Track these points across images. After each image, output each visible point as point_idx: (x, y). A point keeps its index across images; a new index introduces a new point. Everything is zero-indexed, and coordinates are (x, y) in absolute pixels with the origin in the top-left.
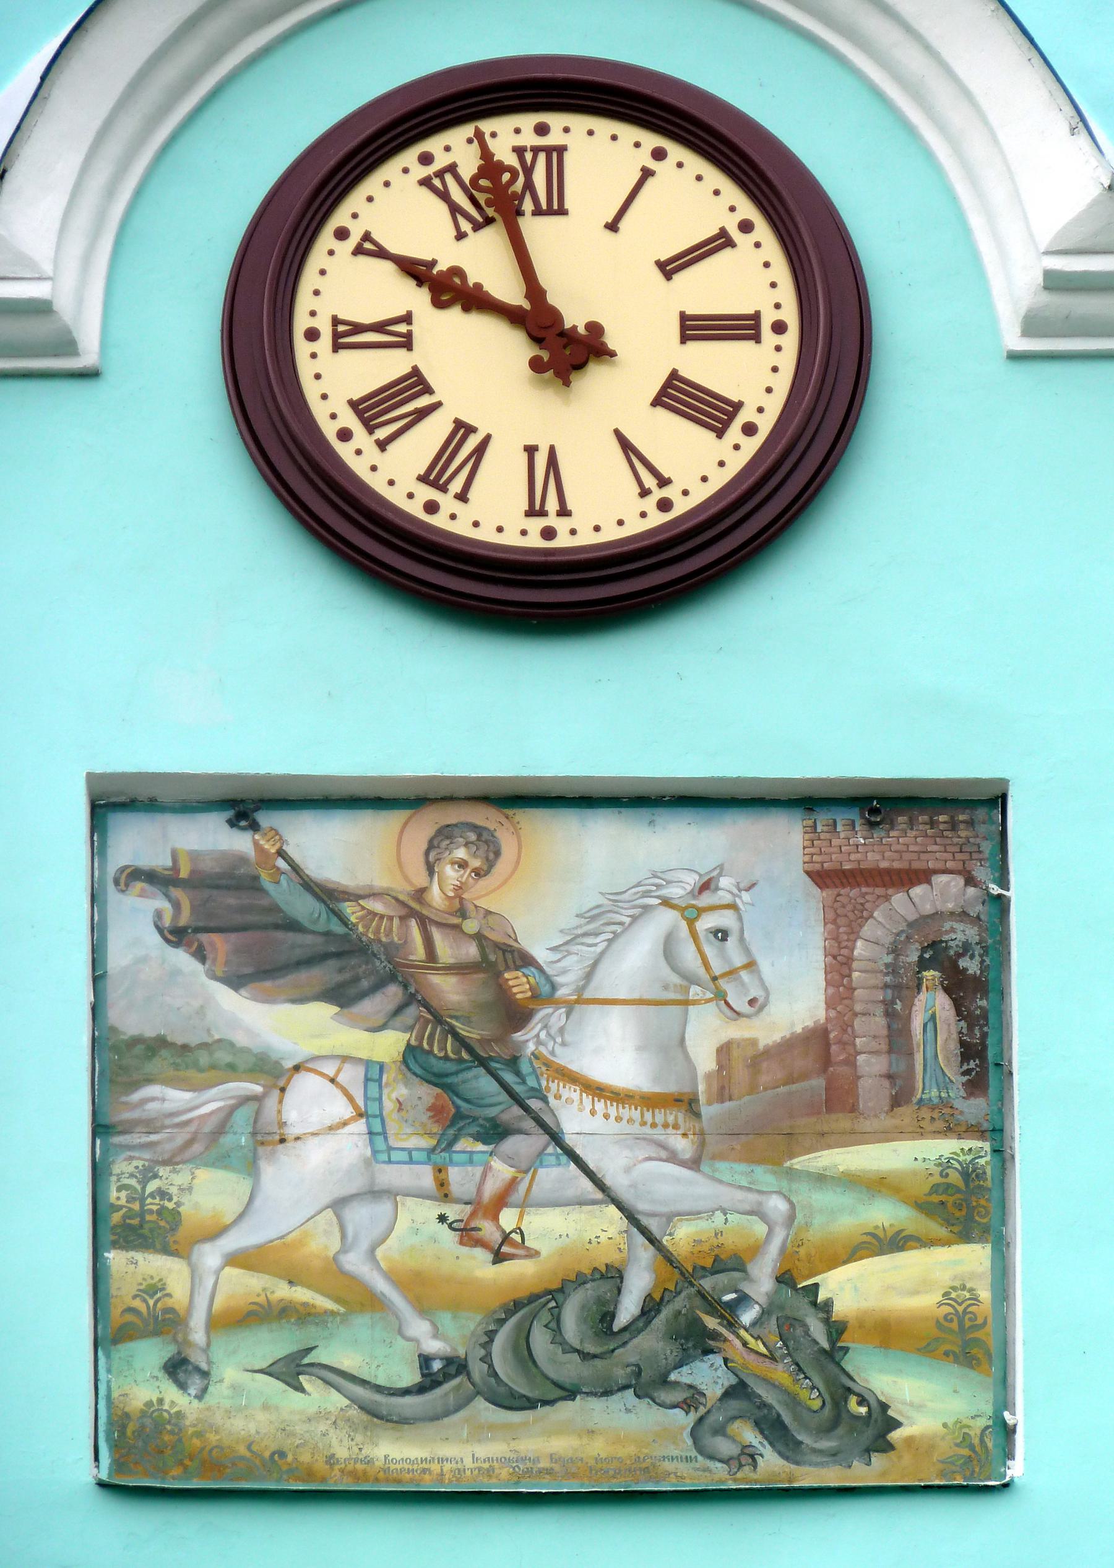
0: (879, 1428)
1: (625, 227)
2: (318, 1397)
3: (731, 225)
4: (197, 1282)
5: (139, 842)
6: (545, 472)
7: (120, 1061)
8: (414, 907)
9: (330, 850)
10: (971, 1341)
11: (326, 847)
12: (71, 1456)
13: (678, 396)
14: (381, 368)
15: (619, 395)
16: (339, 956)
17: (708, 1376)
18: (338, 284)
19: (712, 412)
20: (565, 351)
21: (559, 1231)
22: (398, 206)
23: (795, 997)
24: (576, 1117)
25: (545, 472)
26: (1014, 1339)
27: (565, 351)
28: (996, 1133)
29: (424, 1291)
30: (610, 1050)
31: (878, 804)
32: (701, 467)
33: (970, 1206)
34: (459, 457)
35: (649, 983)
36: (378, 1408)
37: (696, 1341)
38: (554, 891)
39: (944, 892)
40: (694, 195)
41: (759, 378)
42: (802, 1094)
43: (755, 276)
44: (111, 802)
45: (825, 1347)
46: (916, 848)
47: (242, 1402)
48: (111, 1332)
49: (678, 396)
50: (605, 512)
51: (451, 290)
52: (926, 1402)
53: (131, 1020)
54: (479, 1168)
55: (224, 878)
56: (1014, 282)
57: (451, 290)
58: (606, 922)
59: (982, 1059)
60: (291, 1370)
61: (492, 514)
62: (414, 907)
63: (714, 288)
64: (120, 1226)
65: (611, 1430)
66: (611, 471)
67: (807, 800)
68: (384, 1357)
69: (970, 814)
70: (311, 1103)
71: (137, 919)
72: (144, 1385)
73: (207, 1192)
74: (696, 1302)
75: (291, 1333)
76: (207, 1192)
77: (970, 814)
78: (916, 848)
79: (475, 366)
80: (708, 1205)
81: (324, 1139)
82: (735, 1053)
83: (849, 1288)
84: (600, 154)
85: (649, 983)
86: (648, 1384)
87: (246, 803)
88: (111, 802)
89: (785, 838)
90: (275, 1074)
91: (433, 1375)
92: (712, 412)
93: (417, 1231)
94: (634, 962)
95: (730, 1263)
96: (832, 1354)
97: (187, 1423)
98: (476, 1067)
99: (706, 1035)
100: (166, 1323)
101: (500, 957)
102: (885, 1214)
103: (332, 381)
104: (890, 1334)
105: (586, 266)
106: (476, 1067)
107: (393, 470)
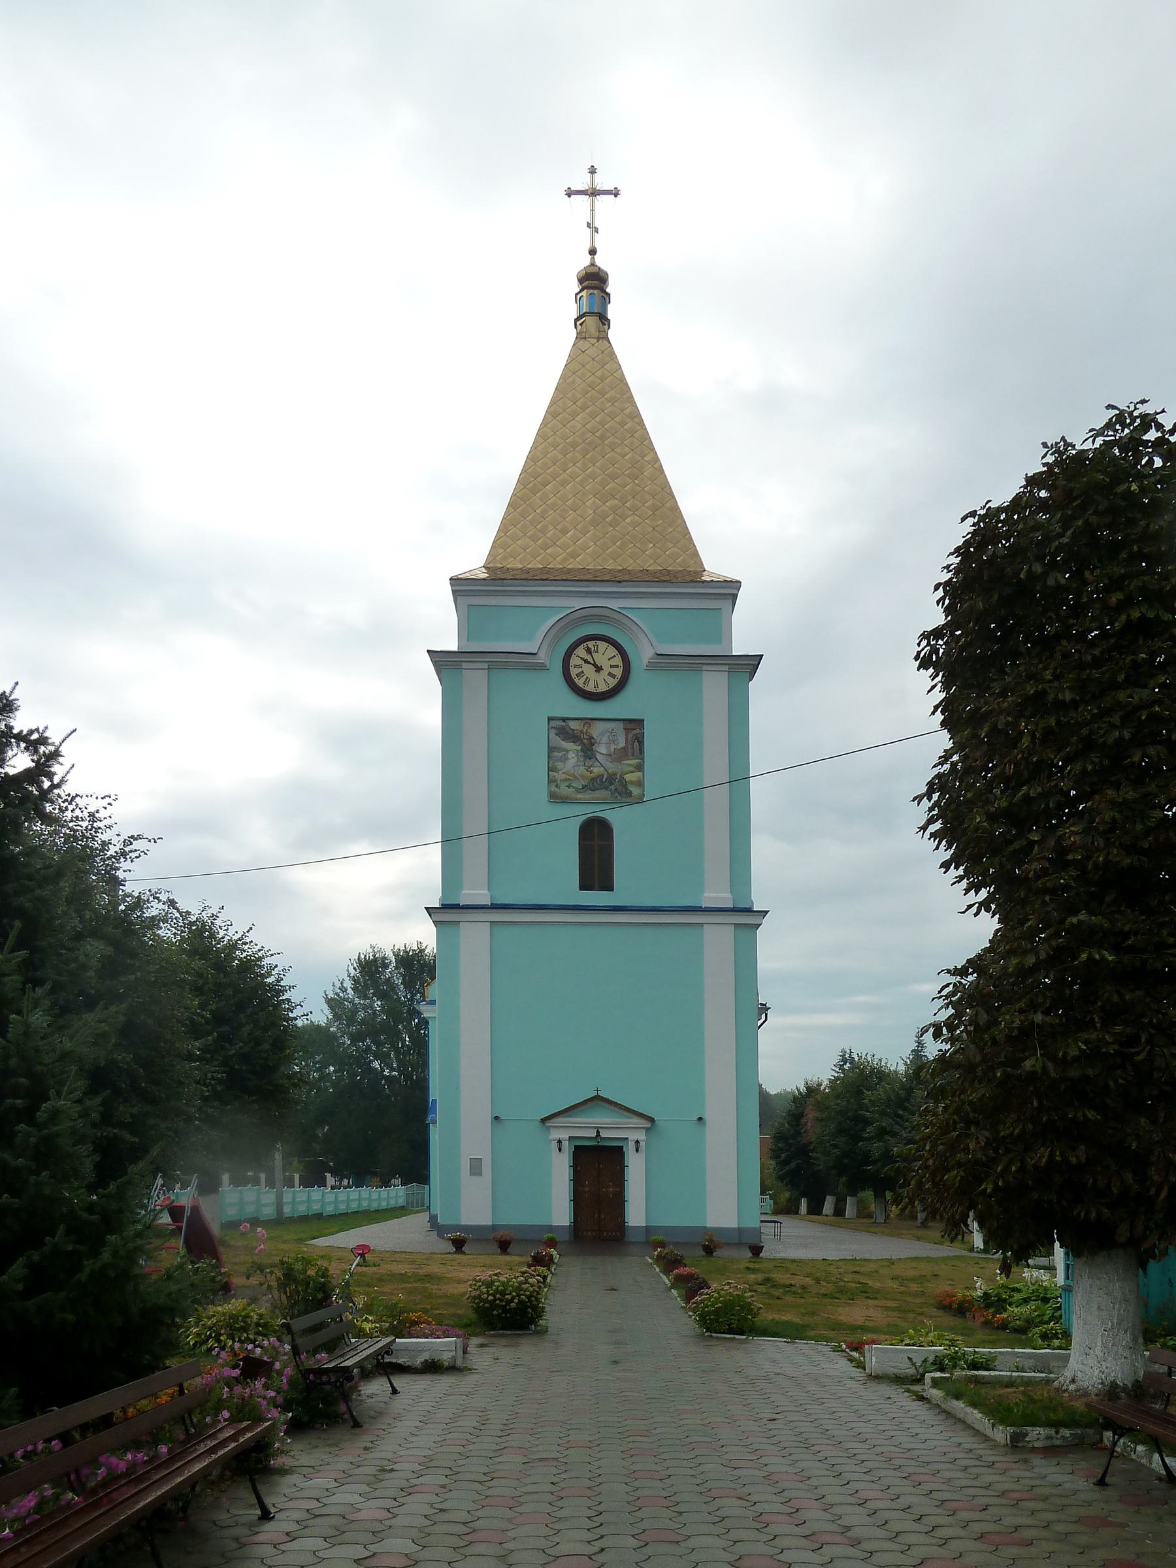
0: (630, 794)
1: (605, 655)
2: (572, 789)
4: (559, 776)
5: (553, 723)
6: (596, 682)
7: (551, 750)
8: (582, 732)
9: (573, 725)
10: (640, 784)
13: (610, 674)
14: (578, 670)
15: (604, 674)
17: (612, 787)
18: (574, 661)
19: (614, 676)
20: (599, 669)
21: (597, 770)
22: (581, 651)
23: (622, 744)
24: (599, 757)
25: (596, 682)
26: (899, 1235)
27: (599, 669)
28: (643, 759)
29: (583, 777)
30: (602, 749)
32: (612, 683)
33: (640, 768)
34: (587, 682)
36: (578, 791)
37: (611, 784)
38: (596, 730)
39: (638, 731)
40: (612, 651)
41: (618, 672)
42: (621, 755)
43: (618, 661)
44: (550, 719)
45: (624, 784)
46: (634, 726)
47: (564, 790)
48: (551, 781)
49: (610, 674)
50: (602, 688)
51: (586, 661)
52: (635, 791)
53: (552, 745)
55: (562, 728)
56: (645, 661)
57: (586, 661)
58: (602, 734)
59: (641, 751)
60: (568, 787)
61: (590, 688)
62: (582, 732)
63: (613, 662)
64: (551, 769)
66: (603, 683)
67: (623, 720)
69: (640, 722)
70: (571, 755)
71: (553, 732)
72: (553, 788)
74: (611, 778)
76: (560, 765)
77: (640, 722)
78: (634, 726)
79: (589, 670)
80: (612, 767)
81: (572, 758)
82: (811, 1114)
83: (628, 777)
84: (602, 645)
86: (606, 788)
87: (564, 720)
88: (550, 719)
89: (621, 725)
90: (567, 751)
92: (614, 676)
94: (605, 740)
95: (615, 774)
96: (625, 786)
98: (588, 750)
99: (613, 747)
100: (555, 781)
101: (591, 738)
102: (632, 769)
103: (574, 672)
104: (631, 782)
105: (600, 659)
106: (588, 750)
107: (580, 682)
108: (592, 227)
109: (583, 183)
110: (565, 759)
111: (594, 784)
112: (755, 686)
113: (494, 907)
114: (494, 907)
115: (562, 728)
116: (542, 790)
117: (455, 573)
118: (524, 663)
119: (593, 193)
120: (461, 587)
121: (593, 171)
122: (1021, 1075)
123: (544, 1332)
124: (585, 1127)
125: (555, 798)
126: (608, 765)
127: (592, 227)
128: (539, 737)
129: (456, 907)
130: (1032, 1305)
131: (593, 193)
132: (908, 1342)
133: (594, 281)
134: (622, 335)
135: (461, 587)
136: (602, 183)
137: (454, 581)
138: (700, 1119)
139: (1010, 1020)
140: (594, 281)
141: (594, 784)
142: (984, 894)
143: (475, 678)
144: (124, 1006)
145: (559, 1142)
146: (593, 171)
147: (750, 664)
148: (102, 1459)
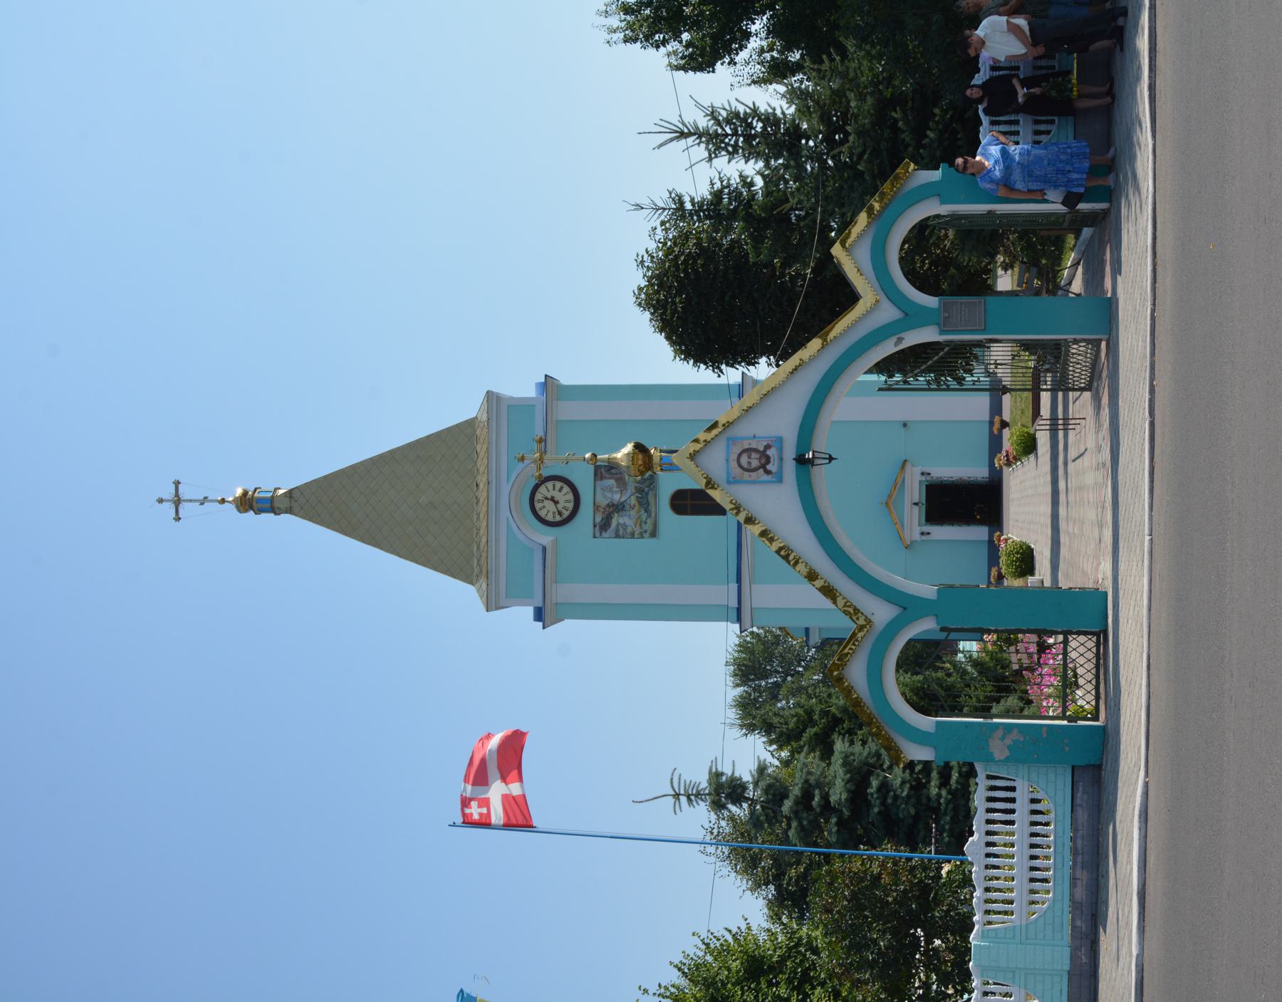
3: (560, 506)
4: (637, 530)
7: (617, 536)
9: (598, 519)
12: (654, 540)
13: (560, 490)
21: (633, 501)
30: (617, 497)
31: (595, 475)
32: (566, 489)
36: (649, 516)
38: (603, 502)
43: (571, 506)
47: (648, 527)
48: (641, 536)
49: (560, 490)
50: (570, 496)
54: (627, 507)
58: (605, 497)
64: (632, 535)
65: (651, 498)
66: (565, 497)
68: (644, 516)
70: (621, 521)
71: (604, 534)
73: (629, 530)
75: (641, 523)
76: (629, 530)
84: (550, 518)
85: (612, 493)
93: (632, 512)
94: (609, 495)
98: (618, 508)
101: (608, 505)
106: (618, 508)
108: (203, 502)
109: (169, 509)
110: (625, 527)
112: (566, 379)
113: (739, 580)
114: (739, 580)
116: (647, 542)
117: (483, 608)
119: (177, 501)
120: (492, 604)
121: (161, 501)
122: (751, 236)
124: (913, 517)
125: (654, 534)
126: (629, 493)
127: (203, 502)
128: (608, 544)
129: (739, 610)
131: (177, 501)
133: (247, 503)
134: (283, 481)
135: (492, 604)
136: (169, 493)
138: (905, 425)
140: (247, 503)
142: (824, 57)
143: (563, 592)
145: (922, 534)
146: (161, 501)
147: (548, 385)
148: (962, 645)
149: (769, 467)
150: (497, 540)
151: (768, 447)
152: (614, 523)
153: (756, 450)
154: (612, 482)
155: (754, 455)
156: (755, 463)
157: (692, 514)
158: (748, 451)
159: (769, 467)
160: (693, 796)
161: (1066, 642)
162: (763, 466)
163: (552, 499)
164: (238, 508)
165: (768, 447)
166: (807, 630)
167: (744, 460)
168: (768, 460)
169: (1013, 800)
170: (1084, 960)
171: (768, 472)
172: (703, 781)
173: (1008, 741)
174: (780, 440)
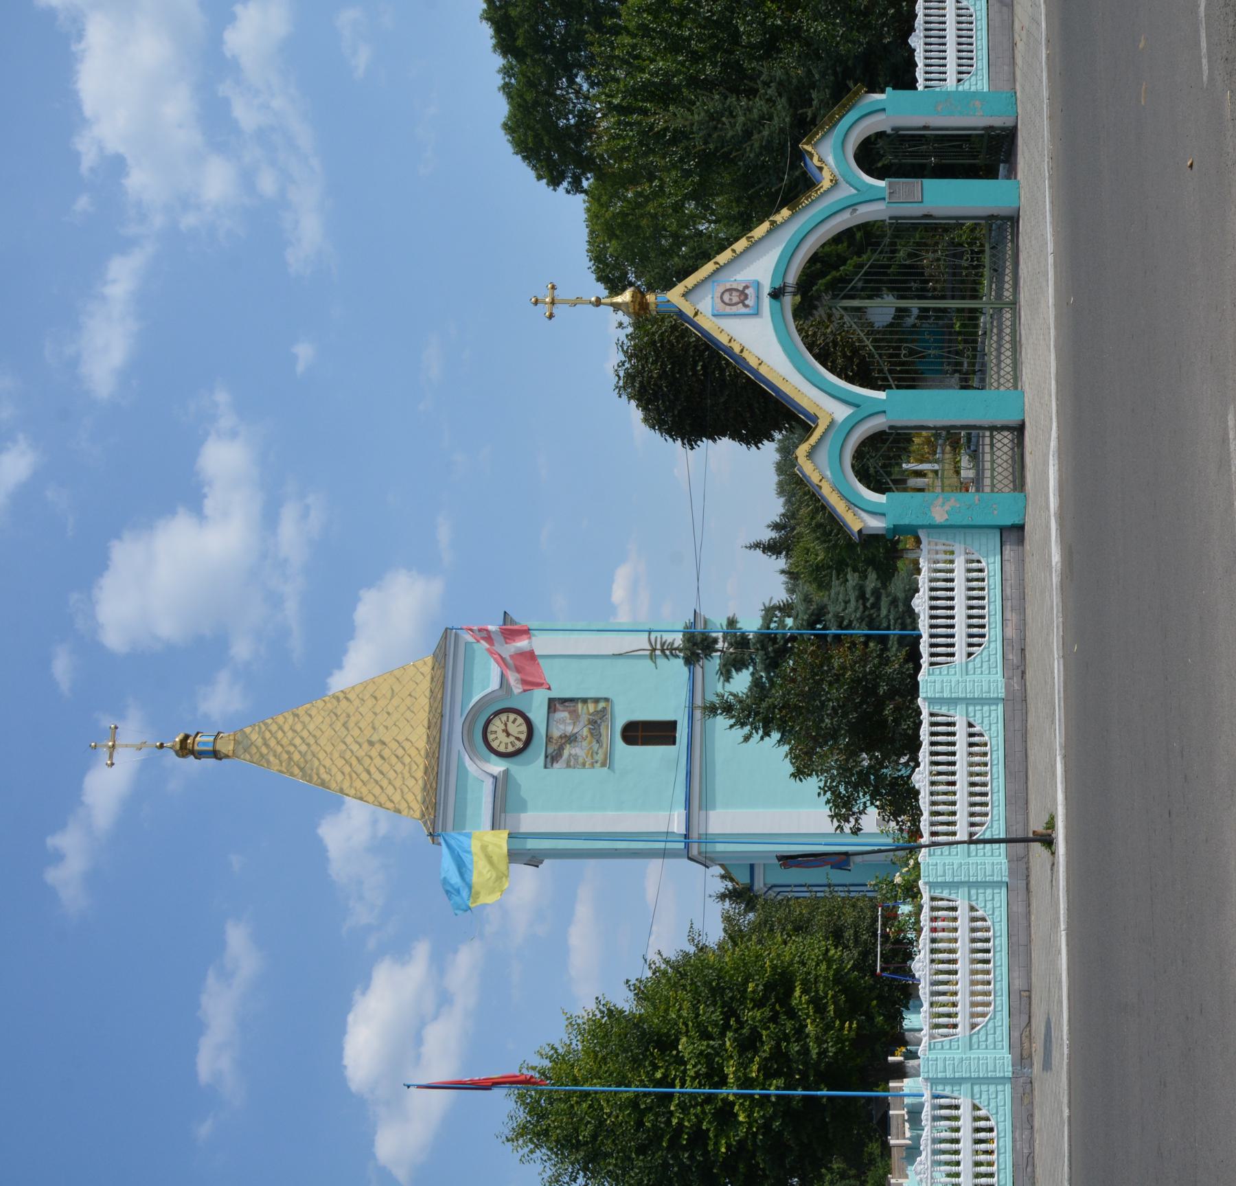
7: (568, 766)
10: (596, 701)
11: (550, 751)
13: (514, 722)
16: (561, 749)
21: (585, 732)
29: (590, 743)
30: (569, 729)
31: (549, 708)
35: (564, 724)
36: (601, 746)
38: (556, 733)
41: (491, 737)
42: (575, 715)
44: (546, 767)
45: (596, 712)
47: (600, 757)
49: (514, 722)
52: (601, 705)
64: (584, 765)
68: (596, 746)
70: (573, 752)
73: (581, 760)
76: (581, 760)
80: (584, 719)
85: (564, 724)
87: (546, 757)
88: (546, 767)
91: (598, 742)
93: (585, 744)
97: (870, 569)
98: (571, 739)
101: (561, 737)
105: (513, 729)
106: (571, 739)
110: (576, 757)
111: (596, 734)
115: (552, 758)
118: (502, 785)
123: (499, 72)
130: (750, 1148)
132: (1047, 397)
137: (674, 743)
139: (529, 97)
141: (596, 734)
144: (711, 1135)
149: (747, 302)
150: (448, 773)
151: (746, 287)
152: (566, 753)
153: (737, 290)
154: (565, 714)
155: (734, 293)
156: (735, 299)
157: (643, 744)
158: (730, 290)
159: (747, 302)
160: (668, 651)
161: (992, 437)
162: (742, 302)
163: (508, 735)
164: (177, 753)
165: (746, 287)
166: (752, 866)
167: (726, 297)
168: (746, 297)
169: (952, 599)
170: (1016, 687)
171: (746, 306)
172: (678, 639)
173: (946, 508)
174: (758, 285)
